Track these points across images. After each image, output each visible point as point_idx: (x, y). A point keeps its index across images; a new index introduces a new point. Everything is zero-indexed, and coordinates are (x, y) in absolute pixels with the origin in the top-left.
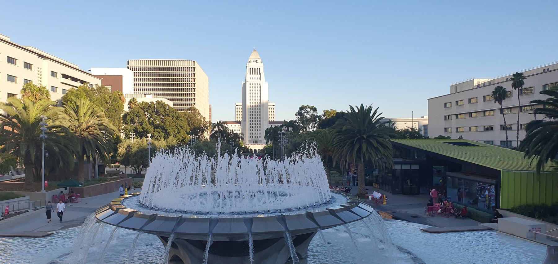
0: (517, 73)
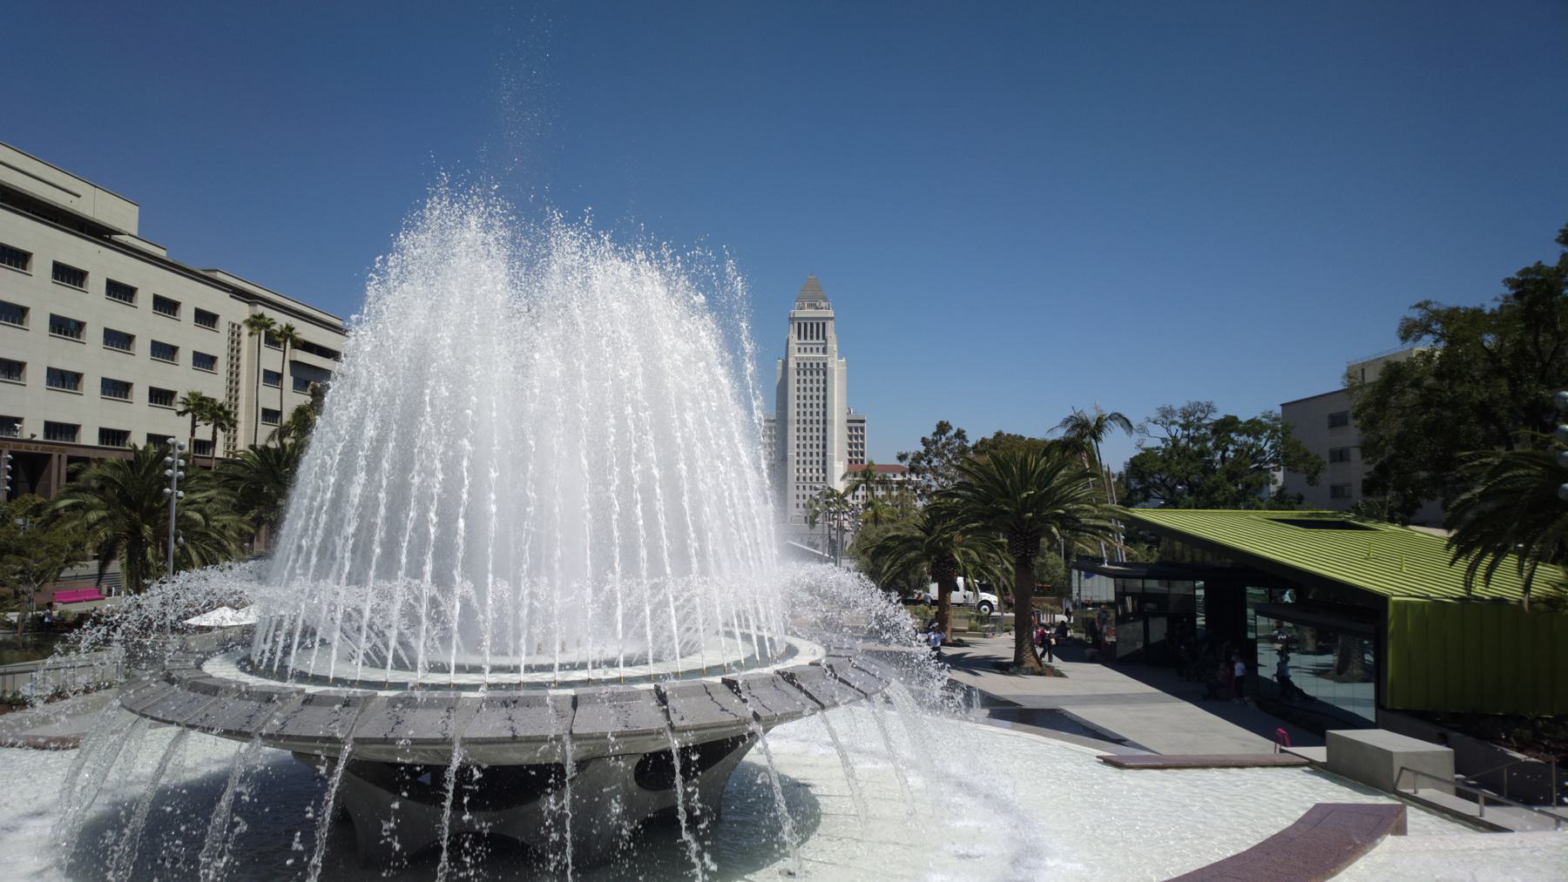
0: (999, 434)
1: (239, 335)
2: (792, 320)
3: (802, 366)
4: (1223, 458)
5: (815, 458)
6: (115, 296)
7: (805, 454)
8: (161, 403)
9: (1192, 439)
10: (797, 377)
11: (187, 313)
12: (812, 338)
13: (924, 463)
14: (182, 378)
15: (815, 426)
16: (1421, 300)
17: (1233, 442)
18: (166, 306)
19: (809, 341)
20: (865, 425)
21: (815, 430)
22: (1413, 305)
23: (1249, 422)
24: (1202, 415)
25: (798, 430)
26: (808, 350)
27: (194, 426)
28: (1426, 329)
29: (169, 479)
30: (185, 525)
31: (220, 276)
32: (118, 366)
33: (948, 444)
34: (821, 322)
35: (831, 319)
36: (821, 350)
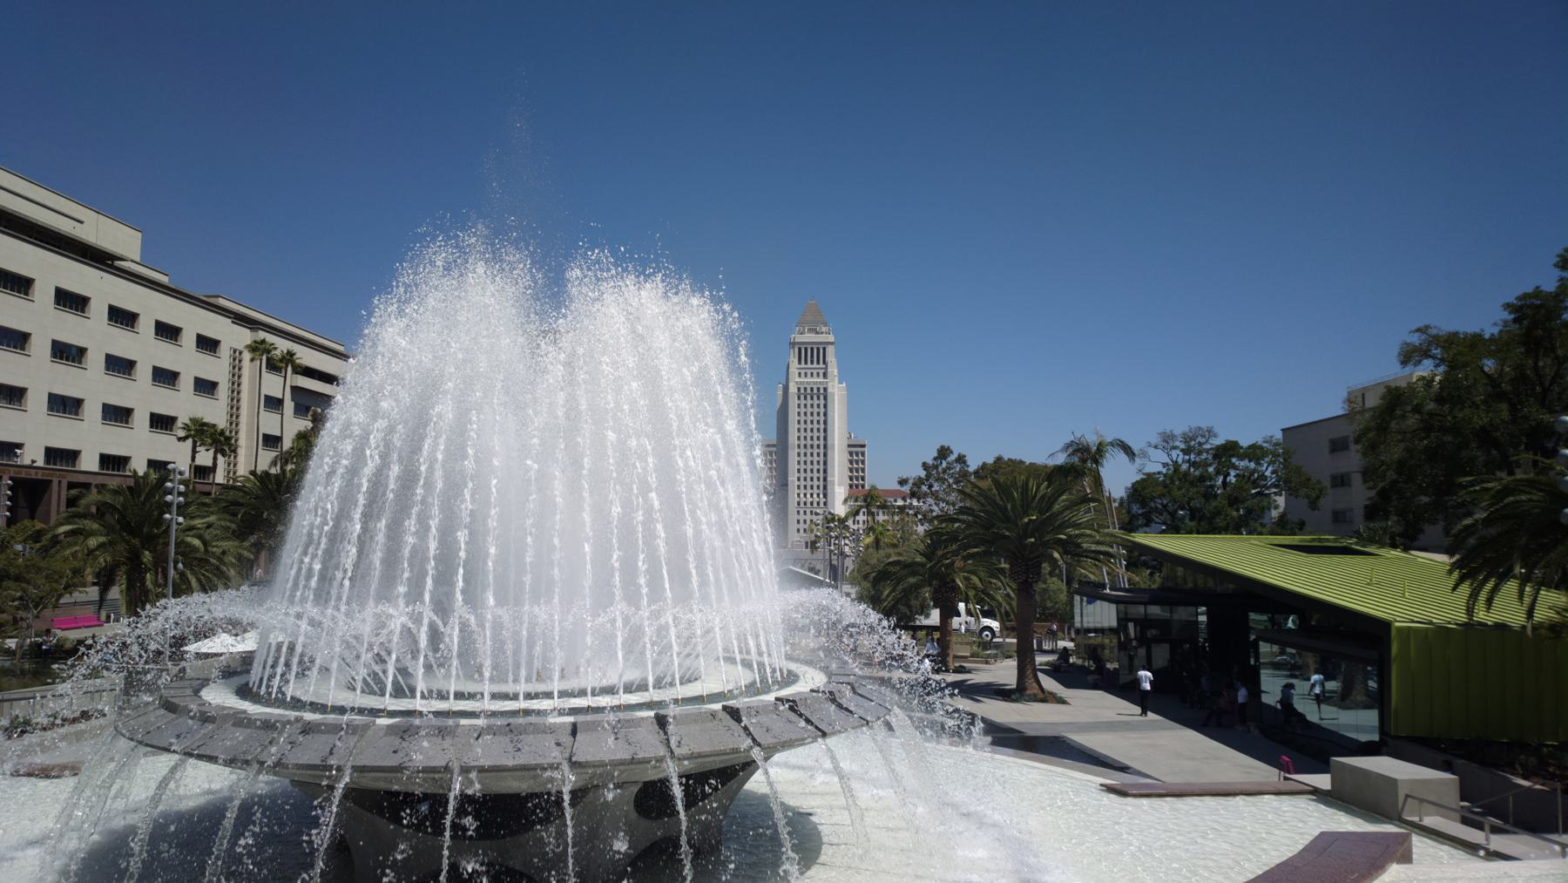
0: (999, 459)
1: (240, 361)
2: (793, 344)
3: (802, 391)
4: (1224, 483)
5: (816, 483)
6: (116, 322)
7: (805, 479)
8: (162, 429)
9: (1193, 464)
10: (797, 402)
11: (188, 339)
12: (812, 362)
13: (924, 488)
14: (183, 404)
15: (816, 451)
16: (1420, 325)
17: (1235, 467)
18: (167, 332)
19: (809, 365)
20: (866, 449)
21: (815, 455)
22: (1413, 329)
23: (1251, 447)
24: (1203, 440)
25: (799, 455)
26: (809, 374)
27: (194, 452)
28: (1426, 354)
29: (169, 505)
30: (184, 550)
31: (222, 302)
32: (119, 391)
33: (949, 469)
34: (821, 347)
35: (832, 343)
36: (821, 375)
